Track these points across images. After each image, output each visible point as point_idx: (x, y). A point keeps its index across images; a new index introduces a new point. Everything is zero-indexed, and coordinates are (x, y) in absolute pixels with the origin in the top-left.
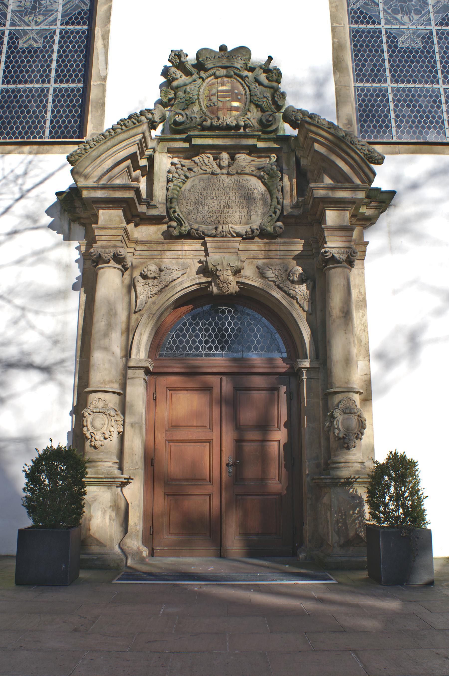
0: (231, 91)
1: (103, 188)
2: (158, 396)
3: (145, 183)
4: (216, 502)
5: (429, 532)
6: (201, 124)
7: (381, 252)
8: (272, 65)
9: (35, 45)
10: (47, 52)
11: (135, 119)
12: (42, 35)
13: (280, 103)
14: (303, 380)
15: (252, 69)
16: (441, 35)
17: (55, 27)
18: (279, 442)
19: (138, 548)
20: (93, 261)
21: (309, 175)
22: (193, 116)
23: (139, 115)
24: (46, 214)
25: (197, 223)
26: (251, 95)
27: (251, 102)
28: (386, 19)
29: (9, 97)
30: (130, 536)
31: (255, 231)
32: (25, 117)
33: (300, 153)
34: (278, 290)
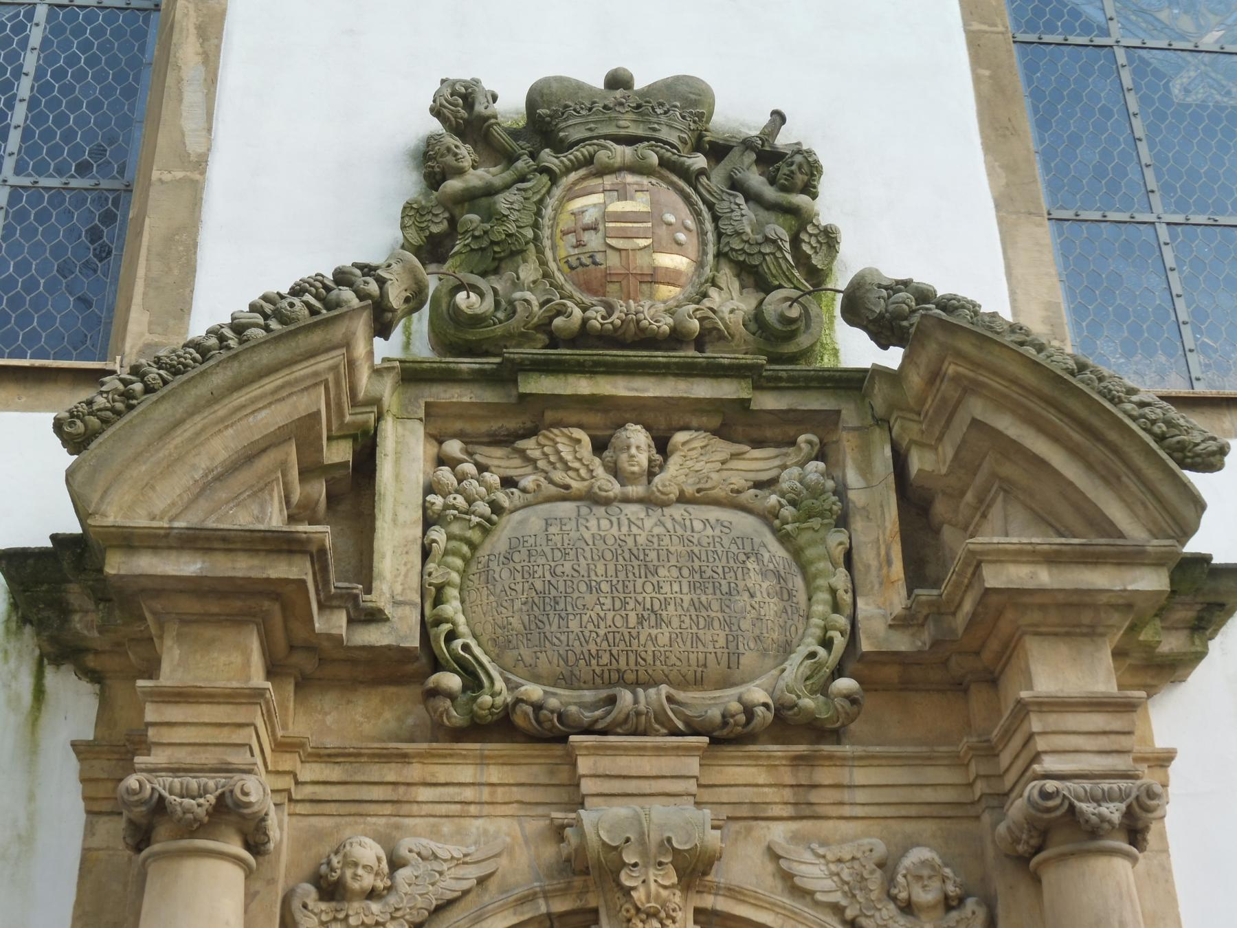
0: (654, 216)
1: (195, 541)
6: (544, 326)
8: (783, 140)
11: (317, 296)
22: (517, 295)
25: (536, 679)
26: (720, 235)
27: (719, 255)
31: (760, 710)
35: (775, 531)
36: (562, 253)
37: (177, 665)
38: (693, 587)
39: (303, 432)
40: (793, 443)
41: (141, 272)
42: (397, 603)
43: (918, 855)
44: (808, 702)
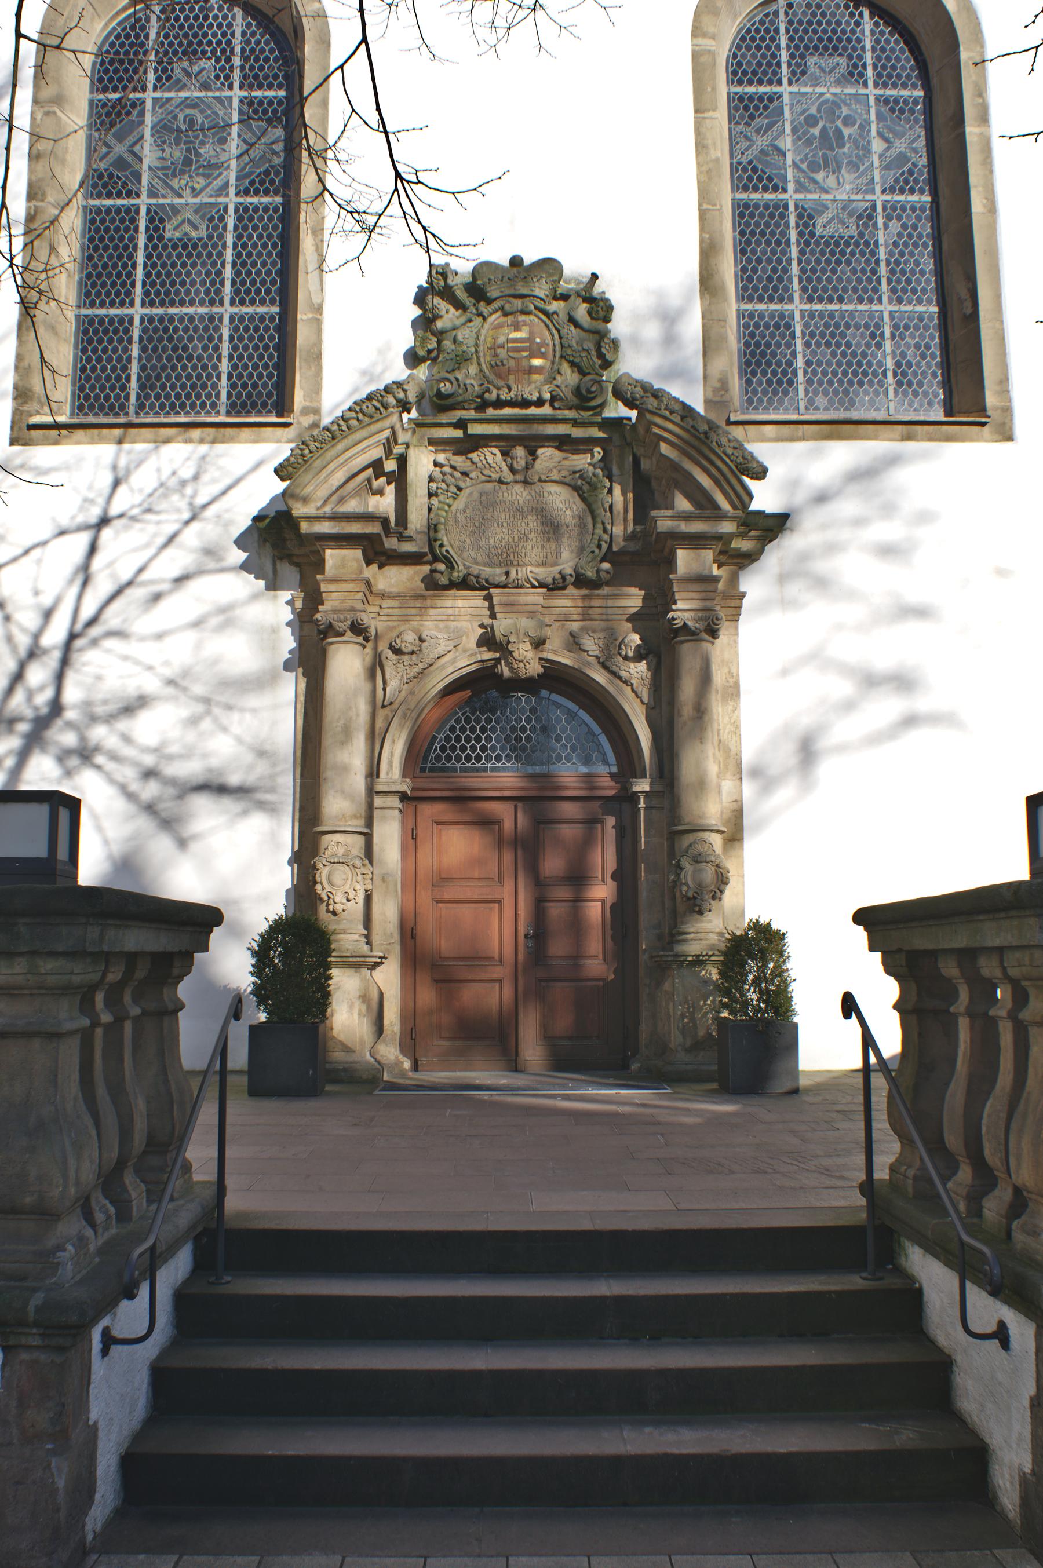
0: (530, 339)
1: (334, 517)
2: (420, 833)
3: (393, 496)
4: (508, 992)
5: (796, 1025)
7: (764, 607)
8: (596, 291)
9: (194, 234)
10: (215, 246)
11: (378, 401)
12: (204, 215)
13: (608, 357)
14: (639, 809)
15: (565, 297)
16: (892, 211)
17: (227, 200)
18: (603, 901)
19: (397, 1057)
20: (320, 632)
21: (654, 484)
23: (383, 393)
24: (235, 547)
25: (477, 563)
27: (562, 357)
28: (797, 182)
29: (156, 330)
30: (384, 1041)
31: (568, 577)
32: (184, 368)
33: (640, 451)
34: (602, 671)
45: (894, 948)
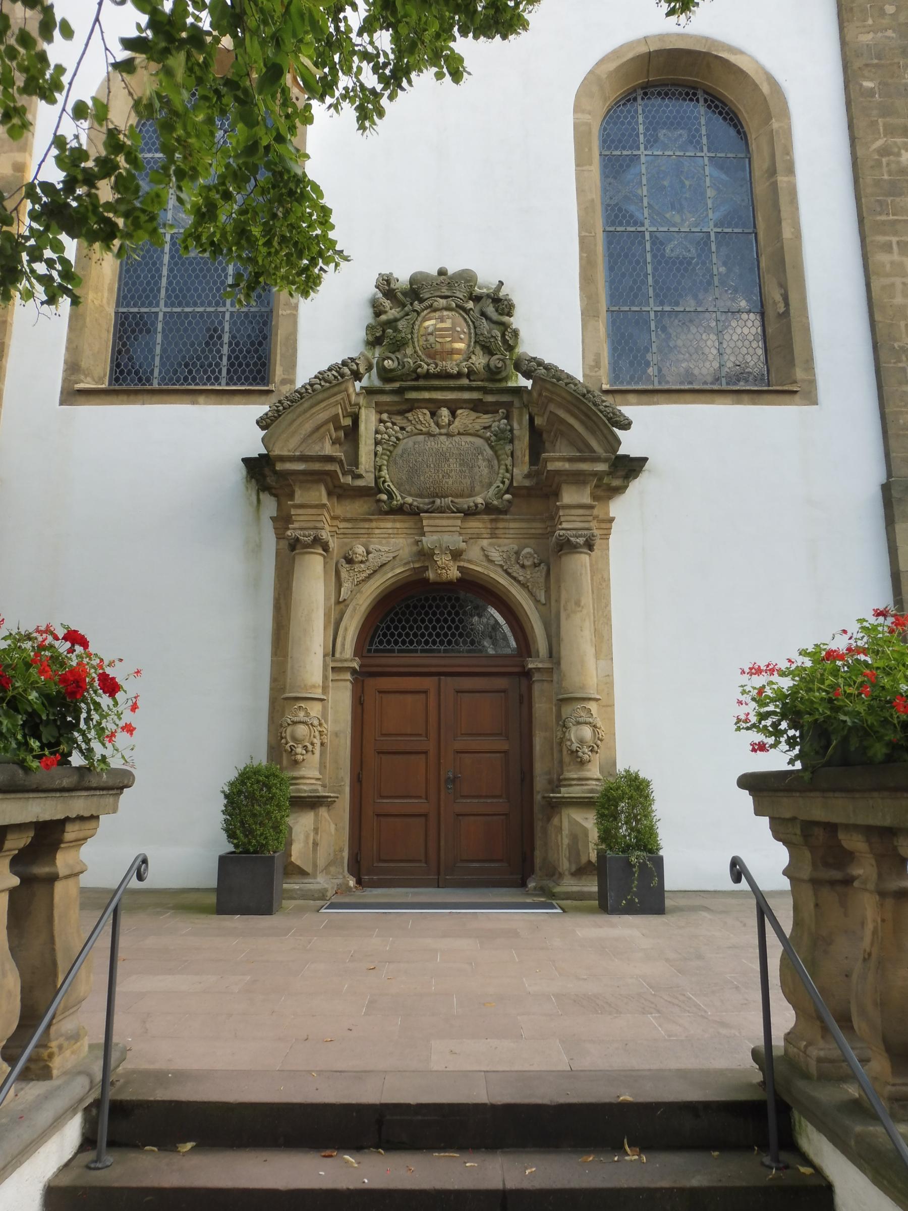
0: (453, 329)
1: (303, 458)
6: (415, 371)
8: (502, 294)
21: (545, 436)
22: (406, 360)
25: (411, 495)
26: (476, 334)
27: (476, 342)
33: (535, 410)
35: (489, 445)
36: (421, 343)
37: (300, 497)
38: (460, 465)
39: (335, 419)
40: (498, 412)
41: (279, 351)
42: (367, 472)
43: (528, 550)
44: (495, 502)
45: (788, 815)
